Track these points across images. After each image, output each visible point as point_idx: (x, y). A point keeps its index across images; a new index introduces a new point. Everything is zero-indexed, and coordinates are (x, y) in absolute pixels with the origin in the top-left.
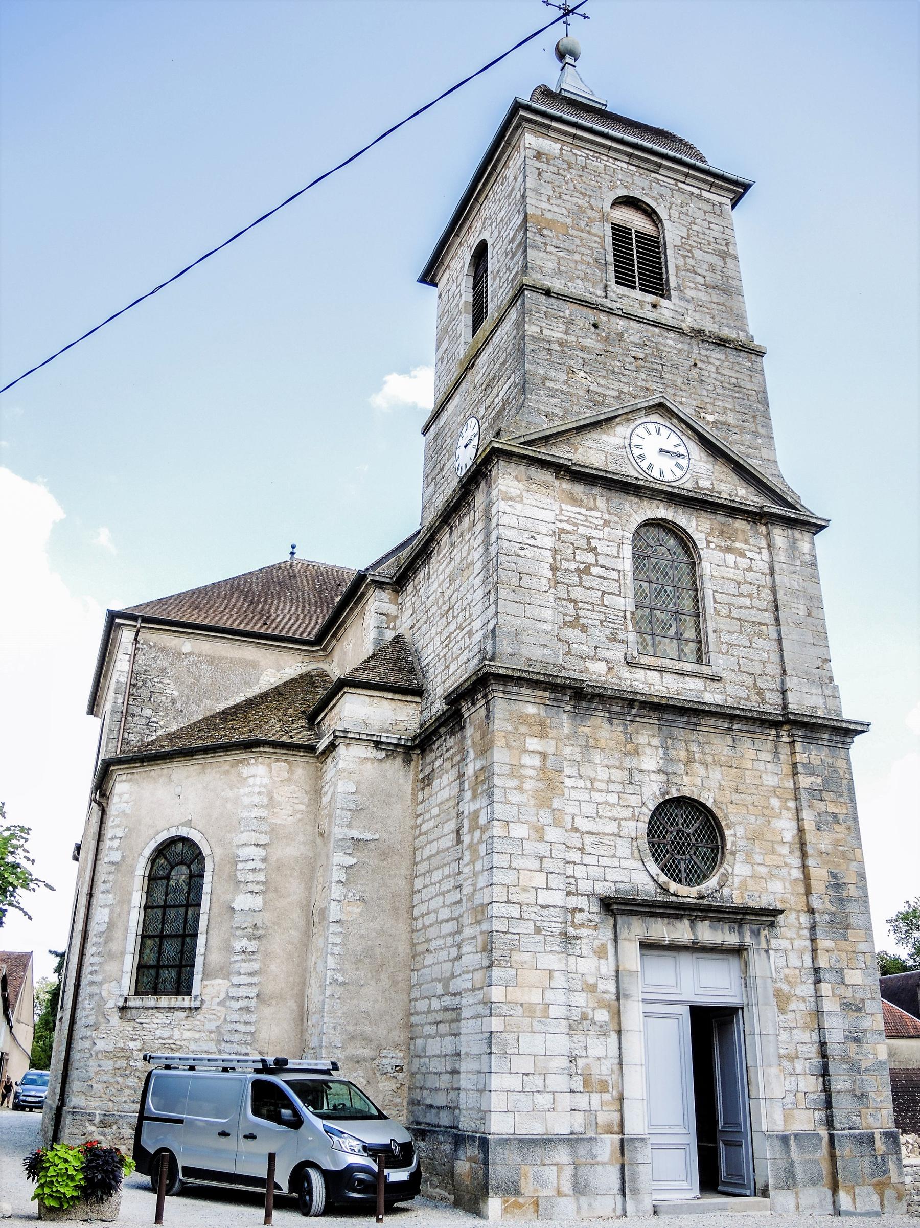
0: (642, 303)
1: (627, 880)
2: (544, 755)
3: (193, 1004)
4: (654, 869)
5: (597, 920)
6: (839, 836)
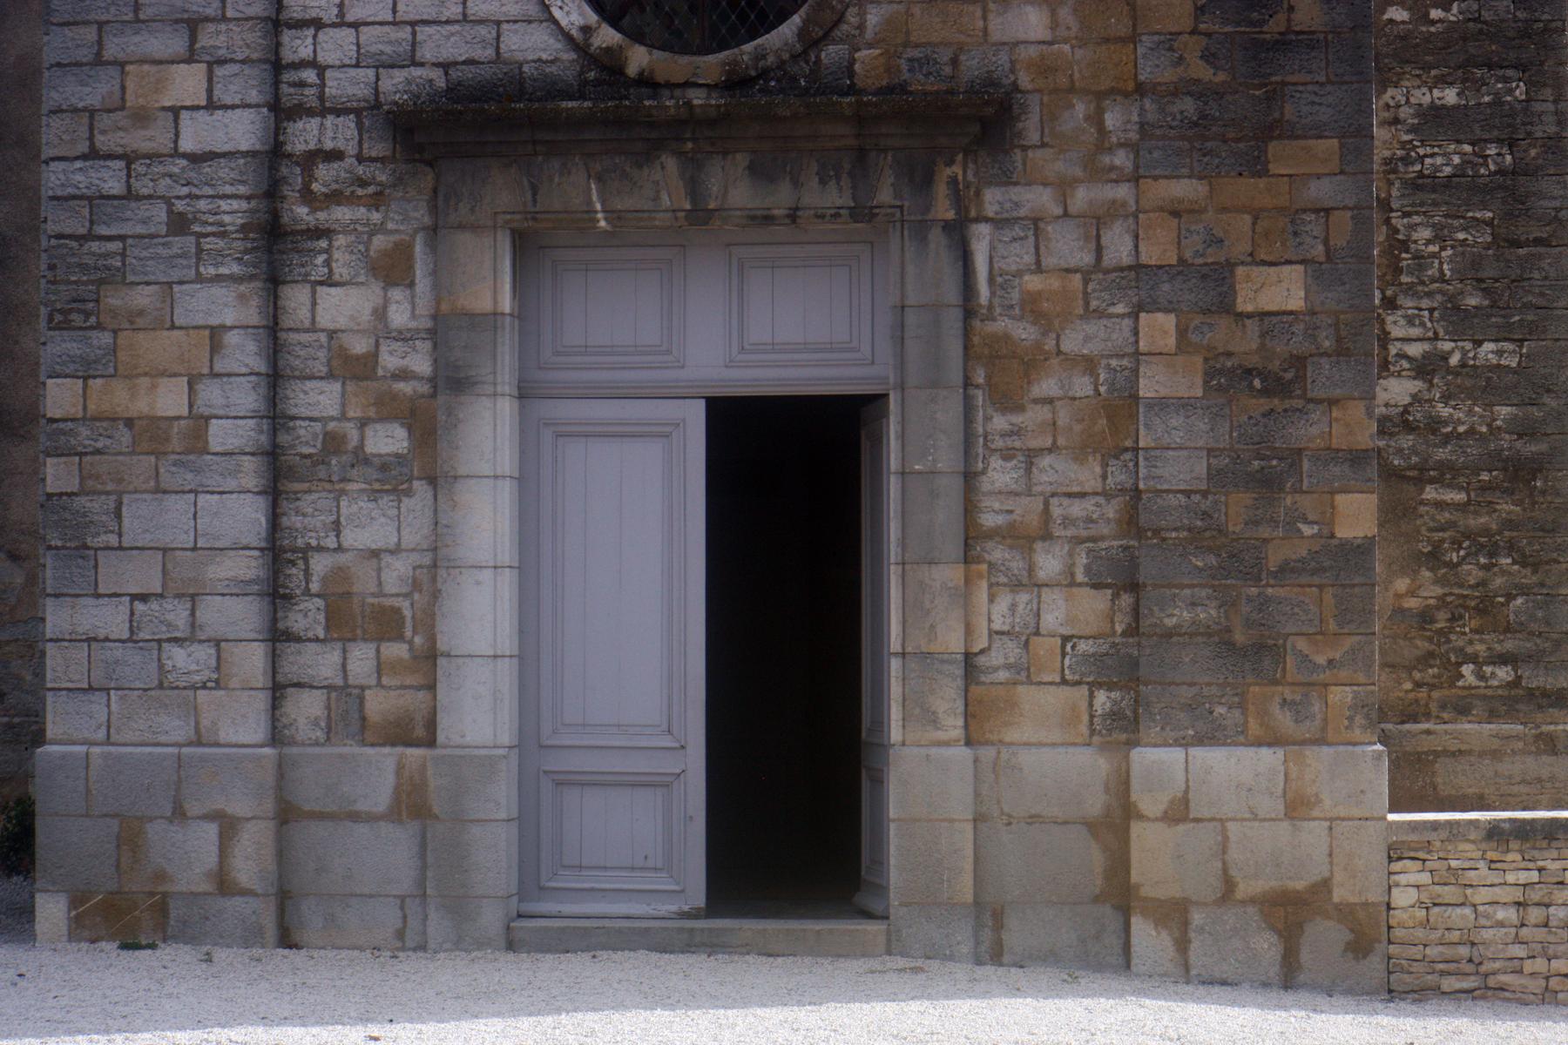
5: (383, 178)
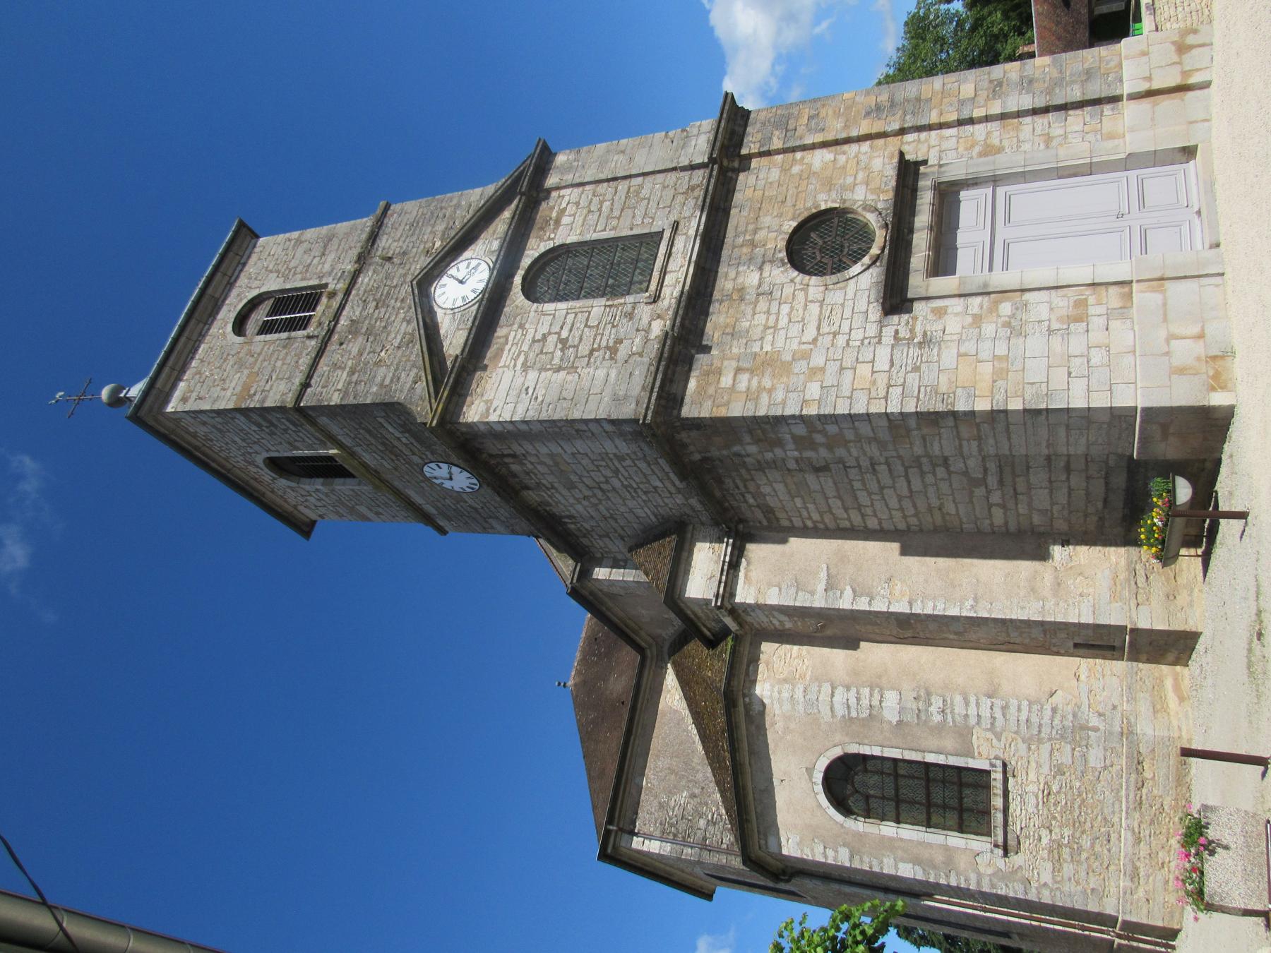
0: (328, 307)
1: (867, 293)
2: (738, 370)
3: (1000, 769)
4: (857, 268)
6: (830, 112)
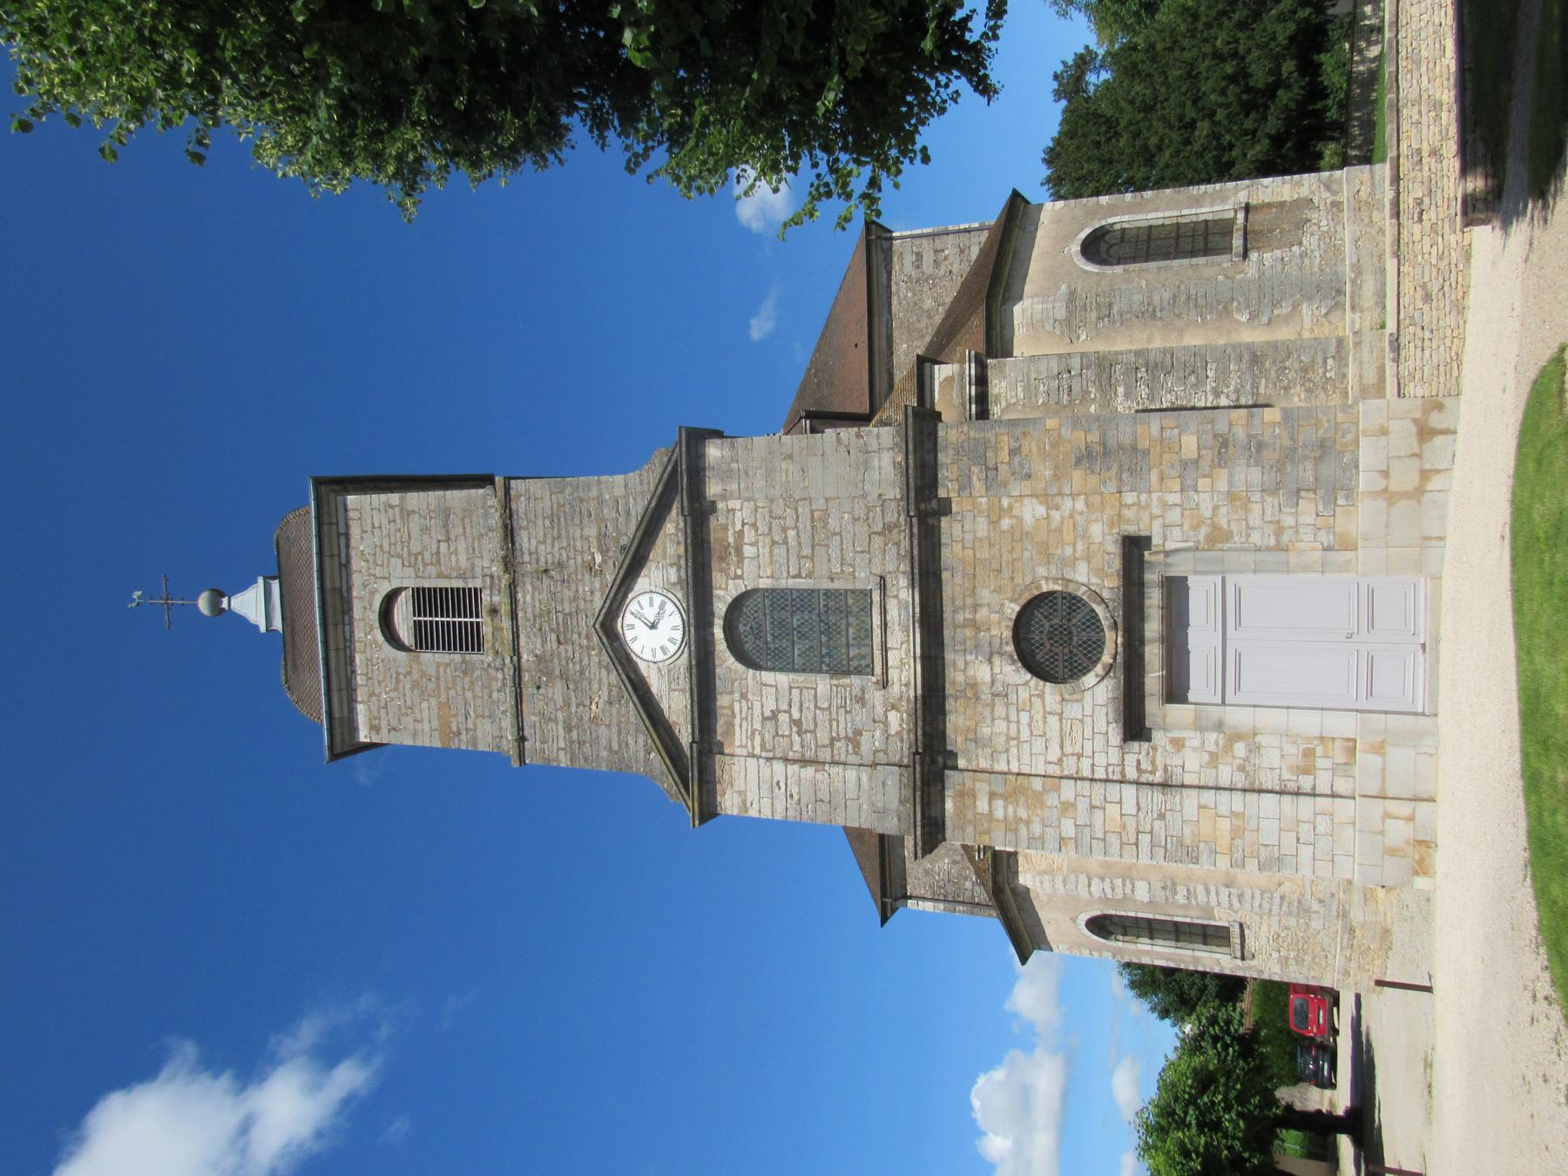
6: (1034, 449)
